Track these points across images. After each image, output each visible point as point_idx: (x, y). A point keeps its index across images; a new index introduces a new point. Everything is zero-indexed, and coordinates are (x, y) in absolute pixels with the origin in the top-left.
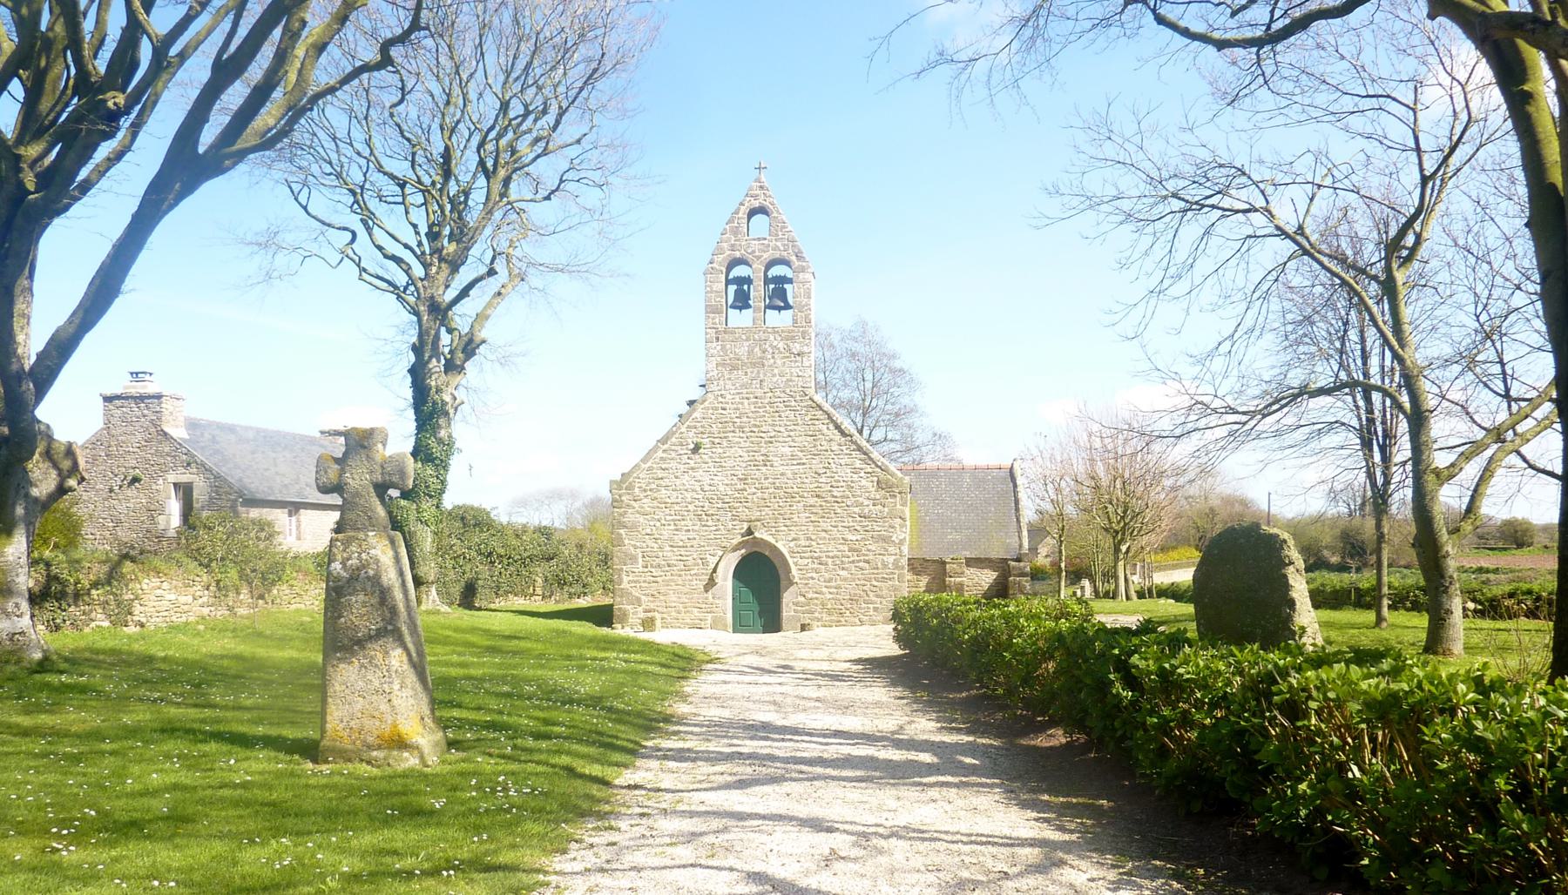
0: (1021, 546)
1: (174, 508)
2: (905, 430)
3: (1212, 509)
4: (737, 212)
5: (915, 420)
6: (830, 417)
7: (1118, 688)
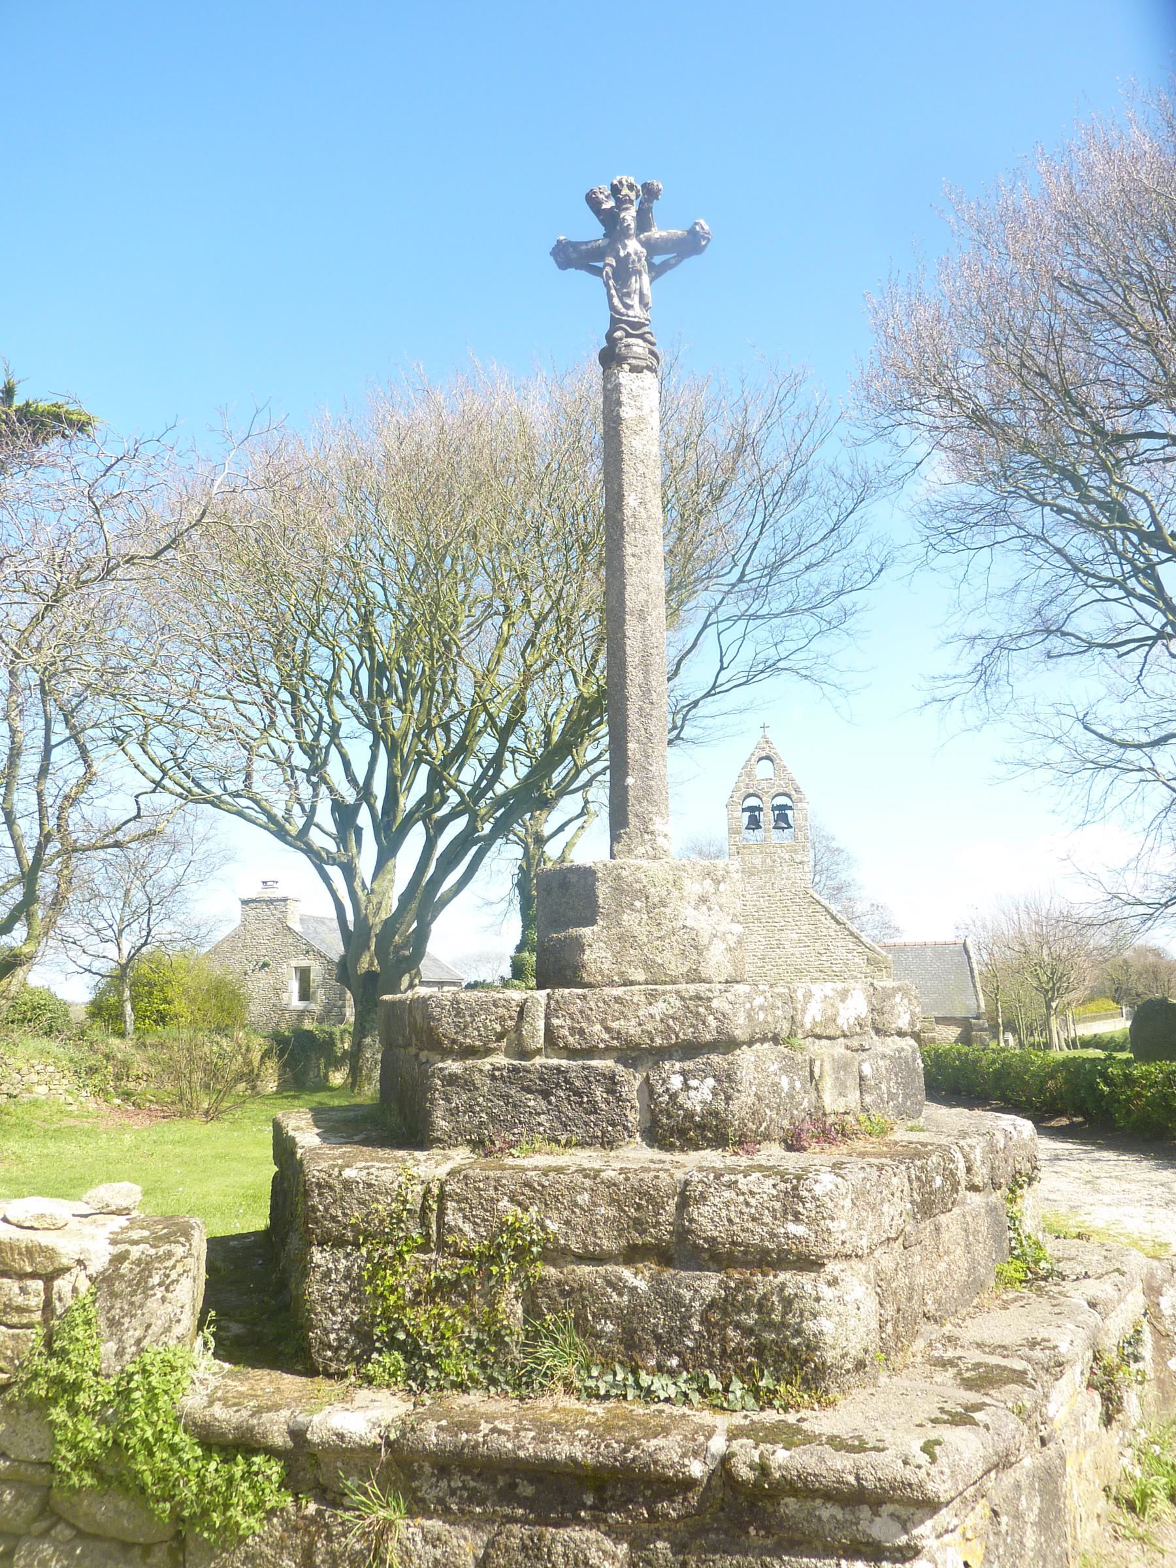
0: (979, 1006)
1: (294, 986)
2: (846, 903)
3: (1125, 961)
4: (749, 761)
5: (853, 892)
6: (827, 910)
7: (1102, 1086)
